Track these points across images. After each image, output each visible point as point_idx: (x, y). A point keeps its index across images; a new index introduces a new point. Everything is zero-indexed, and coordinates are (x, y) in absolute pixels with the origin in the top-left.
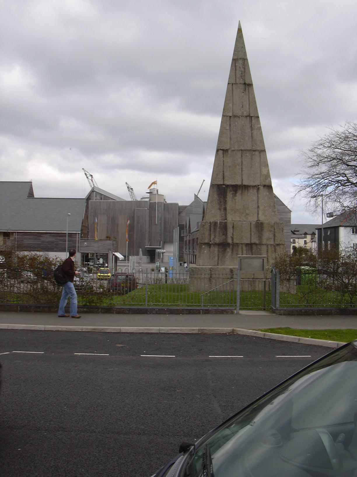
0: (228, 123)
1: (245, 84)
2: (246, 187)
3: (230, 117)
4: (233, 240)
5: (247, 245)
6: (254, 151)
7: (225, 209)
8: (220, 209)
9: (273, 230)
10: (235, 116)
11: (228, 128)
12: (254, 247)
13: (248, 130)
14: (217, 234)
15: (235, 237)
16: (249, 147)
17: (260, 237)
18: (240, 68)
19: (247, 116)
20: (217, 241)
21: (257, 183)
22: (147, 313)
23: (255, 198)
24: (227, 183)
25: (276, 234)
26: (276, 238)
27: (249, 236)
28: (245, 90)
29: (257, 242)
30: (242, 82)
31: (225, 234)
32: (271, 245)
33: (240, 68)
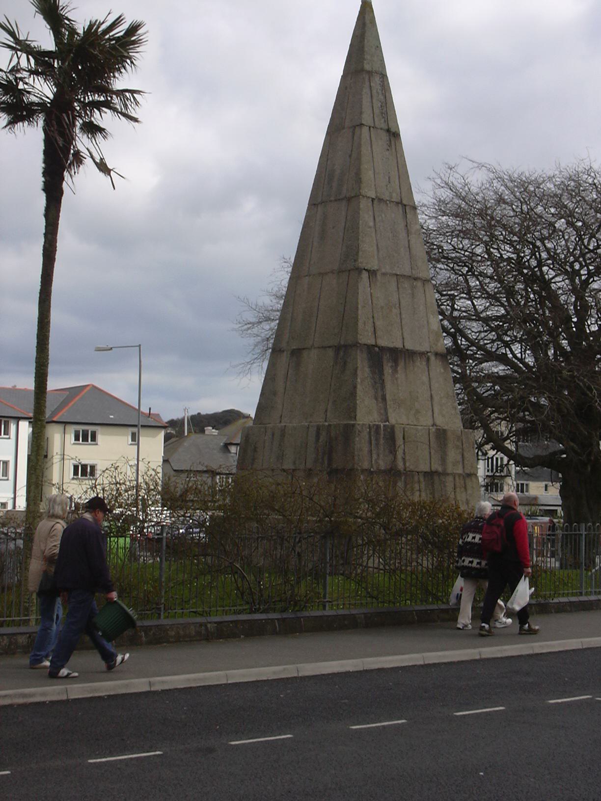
0: (371, 213)
1: (388, 131)
2: (411, 354)
3: (373, 200)
4: (405, 464)
5: (426, 474)
6: (416, 279)
7: (384, 399)
8: (376, 399)
9: (459, 444)
10: (380, 200)
11: (371, 224)
12: (436, 478)
13: (403, 234)
14: (382, 448)
15: (407, 458)
16: (406, 271)
17: (443, 460)
18: (378, 93)
19: (397, 203)
20: (383, 465)
21: (425, 347)
22: (592, 609)
23: (425, 378)
24: (383, 343)
25: (465, 454)
26: (466, 462)
27: (428, 457)
28: (390, 145)
29: (440, 469)
30: (385, 127)
31: (393, 451)
32: (460, 475)
33: (378, 93)
